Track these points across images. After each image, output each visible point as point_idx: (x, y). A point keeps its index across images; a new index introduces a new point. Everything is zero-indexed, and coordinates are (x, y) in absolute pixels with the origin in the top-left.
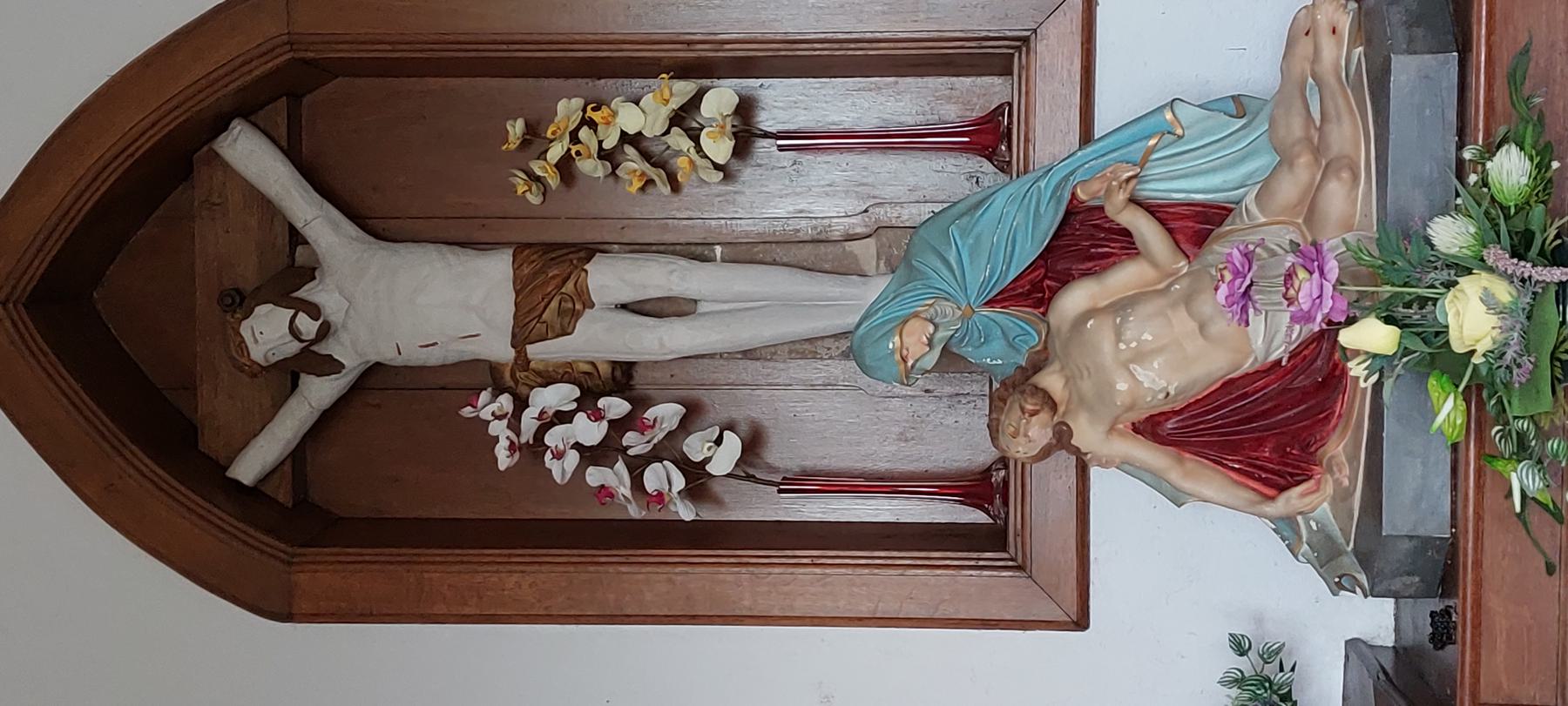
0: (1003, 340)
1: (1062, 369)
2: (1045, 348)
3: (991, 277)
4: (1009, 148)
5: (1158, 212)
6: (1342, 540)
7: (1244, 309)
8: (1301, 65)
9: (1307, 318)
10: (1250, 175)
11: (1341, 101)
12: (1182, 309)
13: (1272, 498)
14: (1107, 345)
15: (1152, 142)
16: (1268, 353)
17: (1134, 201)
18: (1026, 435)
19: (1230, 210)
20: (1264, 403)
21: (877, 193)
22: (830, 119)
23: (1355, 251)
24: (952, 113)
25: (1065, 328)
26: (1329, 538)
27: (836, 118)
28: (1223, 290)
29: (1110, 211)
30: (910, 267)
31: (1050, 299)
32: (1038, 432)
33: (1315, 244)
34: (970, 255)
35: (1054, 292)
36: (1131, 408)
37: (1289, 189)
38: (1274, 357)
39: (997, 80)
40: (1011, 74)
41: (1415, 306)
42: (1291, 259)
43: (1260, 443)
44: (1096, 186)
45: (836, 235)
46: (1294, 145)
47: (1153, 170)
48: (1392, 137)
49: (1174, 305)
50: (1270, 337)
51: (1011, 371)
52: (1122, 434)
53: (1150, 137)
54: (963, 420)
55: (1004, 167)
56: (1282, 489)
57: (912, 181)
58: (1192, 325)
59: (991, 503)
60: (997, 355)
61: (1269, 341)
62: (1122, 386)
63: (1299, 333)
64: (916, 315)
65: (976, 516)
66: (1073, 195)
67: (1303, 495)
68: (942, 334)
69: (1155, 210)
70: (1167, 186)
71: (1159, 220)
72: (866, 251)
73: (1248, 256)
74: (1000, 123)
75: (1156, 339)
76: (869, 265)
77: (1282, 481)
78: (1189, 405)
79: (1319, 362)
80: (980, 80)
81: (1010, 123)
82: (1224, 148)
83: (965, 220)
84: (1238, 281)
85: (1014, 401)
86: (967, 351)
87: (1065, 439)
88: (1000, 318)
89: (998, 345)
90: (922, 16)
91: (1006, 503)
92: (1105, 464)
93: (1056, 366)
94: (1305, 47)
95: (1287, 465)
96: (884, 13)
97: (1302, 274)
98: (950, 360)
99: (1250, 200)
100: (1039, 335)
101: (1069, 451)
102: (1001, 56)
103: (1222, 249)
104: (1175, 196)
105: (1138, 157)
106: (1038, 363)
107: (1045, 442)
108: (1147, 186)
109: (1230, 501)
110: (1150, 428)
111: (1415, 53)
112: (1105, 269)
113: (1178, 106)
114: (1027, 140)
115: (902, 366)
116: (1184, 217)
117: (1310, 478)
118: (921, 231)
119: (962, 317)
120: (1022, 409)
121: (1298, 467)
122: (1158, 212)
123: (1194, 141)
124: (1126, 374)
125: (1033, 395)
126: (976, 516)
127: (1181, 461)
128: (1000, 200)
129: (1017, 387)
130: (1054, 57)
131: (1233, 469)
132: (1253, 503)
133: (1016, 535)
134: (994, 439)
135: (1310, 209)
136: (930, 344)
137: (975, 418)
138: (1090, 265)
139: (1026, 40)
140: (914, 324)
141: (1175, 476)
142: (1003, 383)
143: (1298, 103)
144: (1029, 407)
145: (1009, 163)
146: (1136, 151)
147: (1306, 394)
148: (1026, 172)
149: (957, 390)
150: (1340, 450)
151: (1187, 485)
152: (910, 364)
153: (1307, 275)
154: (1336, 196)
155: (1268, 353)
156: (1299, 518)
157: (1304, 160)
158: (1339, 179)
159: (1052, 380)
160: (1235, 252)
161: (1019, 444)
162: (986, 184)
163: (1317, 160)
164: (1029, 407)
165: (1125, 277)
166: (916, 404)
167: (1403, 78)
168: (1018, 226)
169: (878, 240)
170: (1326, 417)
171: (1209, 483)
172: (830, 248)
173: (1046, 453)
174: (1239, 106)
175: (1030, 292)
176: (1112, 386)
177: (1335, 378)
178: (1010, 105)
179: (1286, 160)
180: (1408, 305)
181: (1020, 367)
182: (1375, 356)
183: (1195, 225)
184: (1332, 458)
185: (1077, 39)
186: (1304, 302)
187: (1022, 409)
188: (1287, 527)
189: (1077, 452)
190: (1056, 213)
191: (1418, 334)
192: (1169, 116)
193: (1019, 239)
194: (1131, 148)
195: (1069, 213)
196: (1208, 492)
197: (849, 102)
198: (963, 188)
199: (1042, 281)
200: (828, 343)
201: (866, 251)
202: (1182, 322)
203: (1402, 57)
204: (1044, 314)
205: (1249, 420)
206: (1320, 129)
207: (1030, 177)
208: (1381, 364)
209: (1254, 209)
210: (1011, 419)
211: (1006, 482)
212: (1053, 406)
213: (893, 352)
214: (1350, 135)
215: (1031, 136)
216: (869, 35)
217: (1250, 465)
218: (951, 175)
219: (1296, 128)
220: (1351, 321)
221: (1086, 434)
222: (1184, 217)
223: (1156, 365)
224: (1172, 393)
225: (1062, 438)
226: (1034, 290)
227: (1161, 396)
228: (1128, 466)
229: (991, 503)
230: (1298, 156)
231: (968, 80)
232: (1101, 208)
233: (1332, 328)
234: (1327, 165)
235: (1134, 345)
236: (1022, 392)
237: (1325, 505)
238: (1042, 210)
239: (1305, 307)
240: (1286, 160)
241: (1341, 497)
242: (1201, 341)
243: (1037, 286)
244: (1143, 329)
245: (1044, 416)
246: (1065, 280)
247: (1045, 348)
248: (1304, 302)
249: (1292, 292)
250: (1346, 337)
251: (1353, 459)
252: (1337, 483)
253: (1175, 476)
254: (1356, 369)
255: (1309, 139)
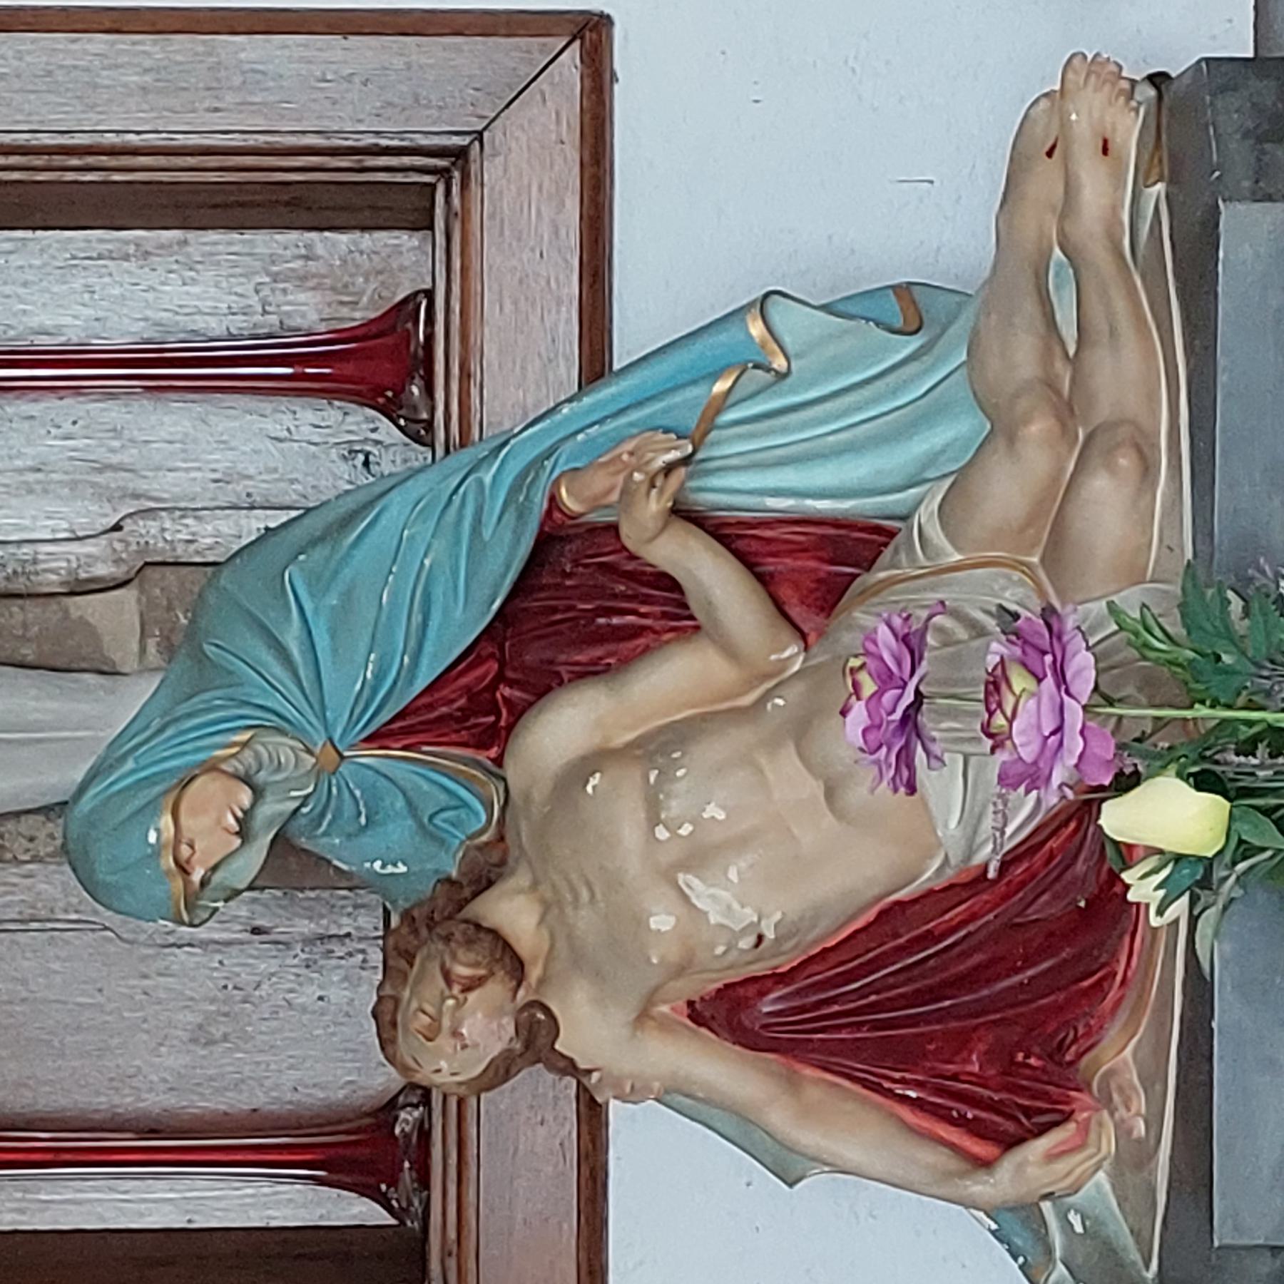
0: (409, 818)
1: (535, 884)
2: (501, 838)
3: (379, 676)
4: (429, 390)
5: (734, 536)
6: (1135, 1256)
7: (905, 758)
8: (1037, 221)
9: (1033, 777)
10: (933, 459)
11: (1121, 306)
12: (791, 749)
13: (985, 1164)
14: (630, 833)
15: (721, 386)
16: (970, 852)
17: (684, 513)
18: (456, 1034)
19: (891, 534)
20: (965, 955)
21: (143, 486)
22: (34, 322)
23: (1137, 633)
24: (308, 311)
25: (539, 794)
26: (1109, 1251)
27: (48, 321)
28: (859, 712)
29: (629, 536)
30: (201, 658)
31: (510, 728)
32: (484, 1026)
33: (1049, 613)
34: (333, 634)
35: (518, 712)
36: (680, 970)
37: (1008, 490)
38: (978, 859)
39: (407, 240)
40: (431, 227)
41: (1262, 750)
42: (998, 648)
43: (961, 1042)
44: (598, 482)
45: (51, 582)
46: (1017, 395)
47: (725, 447)
48: (1222, 378)
49: (772, 745)
50: (962, 816)
51: (425, 888)
52: (665, 1025)
53: (716, 376)
54: (338, 995)
55: (420, 432)
56: (1010, 1143)
57: (221, 460)
58: (816, 788)
59: (393, 1183)
60: (398, 855)
61: (972, 822)
62: (661, 922)
63: (1024, 813)
64: (212, 767)
65: (357, 1210)
66: (554, 500)
67: (1052, 1157)
68: (273, 808)
69: (728, 533)
70: (748, 481)
71: (741, 556)
72: (116, 617)
73: (912, 644)
74: (408, 337)
75: (733, 818)
76: (125, 649)
77: (1010, 1127)
78: (811, 960)
79: (1080, 867)
80: (367, 240)
81: (430, 337)
82: (876, 401)
83: (320, 553)
84: (889, 696)
85: (430, 956)
86: (330, 844)
87: (542, 1041)
88: (401, 772)
89: (398, 832)
90: (230, 99)
91: (424, 1181)
92: (633, 1095)
93: (521, 879)
94: (1045, 182)
95: (1021, 1090)
96: (144, 89)
97: (1020, 681)
98: (292, 863)
99: (927, 516)
100: (489, 808)
101: (551, 1068)
102: (415, 188)
103: (868, 623)
104: (771, 502)
105: (691, 421)
106: (483, 875)
107: (496, 1049)
108: (715, 482)
109: (899, 1173)
110: (726, 1012)
111: (1270, 198)
112: (626, 662)
113: (777, 309)
114: (465, 374)
115: (179, 883)
116: (797, 550)
117: (1067, 1117)
118: (226, 572)
119: (317, 772)
120: (447, 976)
121: (1045, 1096)
122: (734, 536)
123: (812, 384)
124: (672, 894)
125: (469, 943)
126: (357, 1210)
127: (793, 1084)
128: (397, 507)
129: (439, 924)
130: (524, 193)
131: (904, 1099)
132: (948, 1175)
133: (445, 1254)
134: (386, 1043)
135: (1053, 536)
136: (244, 831)
137: (352, 987)
138: (598, 652)
139: (460, 154)
140: (204, 786)
141: (779, 1117)
142: (407, 916)
143: (1030, 306)
144: (461, 971)
145: (429, 425)
146: (685, 406)
147: (1052, 939)
148: (462, 445)
149: (324, 925)
150: (1127, 1055)
151: (809, 1138)
152: (197, 876)
153: (1030, 684)
154: (1106, 506)
155: (970, 852)
156: (1046, 1206)
157: (1038, 428)
158: (1112, 469)
159: (512, 911)
160: (884, 633)
161: (439, 1054)
162: (387, 468)
163: (1066, 432)
164: (461, 971)
165: (669, 680)
166: (232, 958)
167: (1247, 251)
168: (437, 577)
169: (142, 591)
170: (1099, 983)
171: (851, 1128)
172: (33, 610)
173: (501, 1072)
174: (909, 309)
175: (466, 713)
176: (640, 922)
177: (1108, 908)
178: (430, 294)
179: (1002, 431)
180: (1248, 748)
181: (449, 881)
182: (1178, 858)
183: (811, 567)
184: (1111, 1073)
185: (571, 155)
186: (1025, 745)
187: (447, 976)
188: (1020, 1226)
189: (569, 1067)
190: (517, 541)
191: (1267, 812)
192: (756, 329)
193: (438, 592)
194: (677, 398)
195: (547, 542)
196: (852, 1153)
197: (77, 284)
198: (336, 478)
199: (493, 687)
200: (26, 825)
201: (116, 617)
202: (790, 780)
203: (1240, 207)
204: (499, 761)
205: (934, 994)
206: (1075, 362)
207: (464, 457)
208: (1195, 876)
209: (936, 534)
210: (424, 996)
211: (424, 1133)
212: (517, 968)
213: (157, 850)
214: (1135, 374)
215: (474, 367)
216: (111, 139)
217: (940, 1091)
218: (301, 447)
219: (1022, 356)
220: (1125, 783)
221: (589, 1029)
222: (797, 550)
223: (733, 875)
224: (770, 935)
225: (536, 1038)
226: (475, 705)
227: (746, 943)
228: (678, 1096)
229: (393, 1183)
230: (1027, 421)
231: (343, 239)
232: (613, 529)
233: (1085, 809)
234: (1089, 438)
235: (686, 830)
236: (447, 939)
237: (1101, 1176)
238: (487, 533)
239: (1028, 754)
240: (1002, 431)
241: (1133, 1159)
242: (829, 818)
243: (481, 701)
244: (706, 796)
245: (496, 990)
246: (543, 685)
247: (501, 838)
248: (1025, 745)
249: (999, 720)
250: (1116, 818)
251: (1151, 1080)
252: (1123, 1131)
253: (779, 1117)
254: (1142, 887)
255: (1050, 384)
